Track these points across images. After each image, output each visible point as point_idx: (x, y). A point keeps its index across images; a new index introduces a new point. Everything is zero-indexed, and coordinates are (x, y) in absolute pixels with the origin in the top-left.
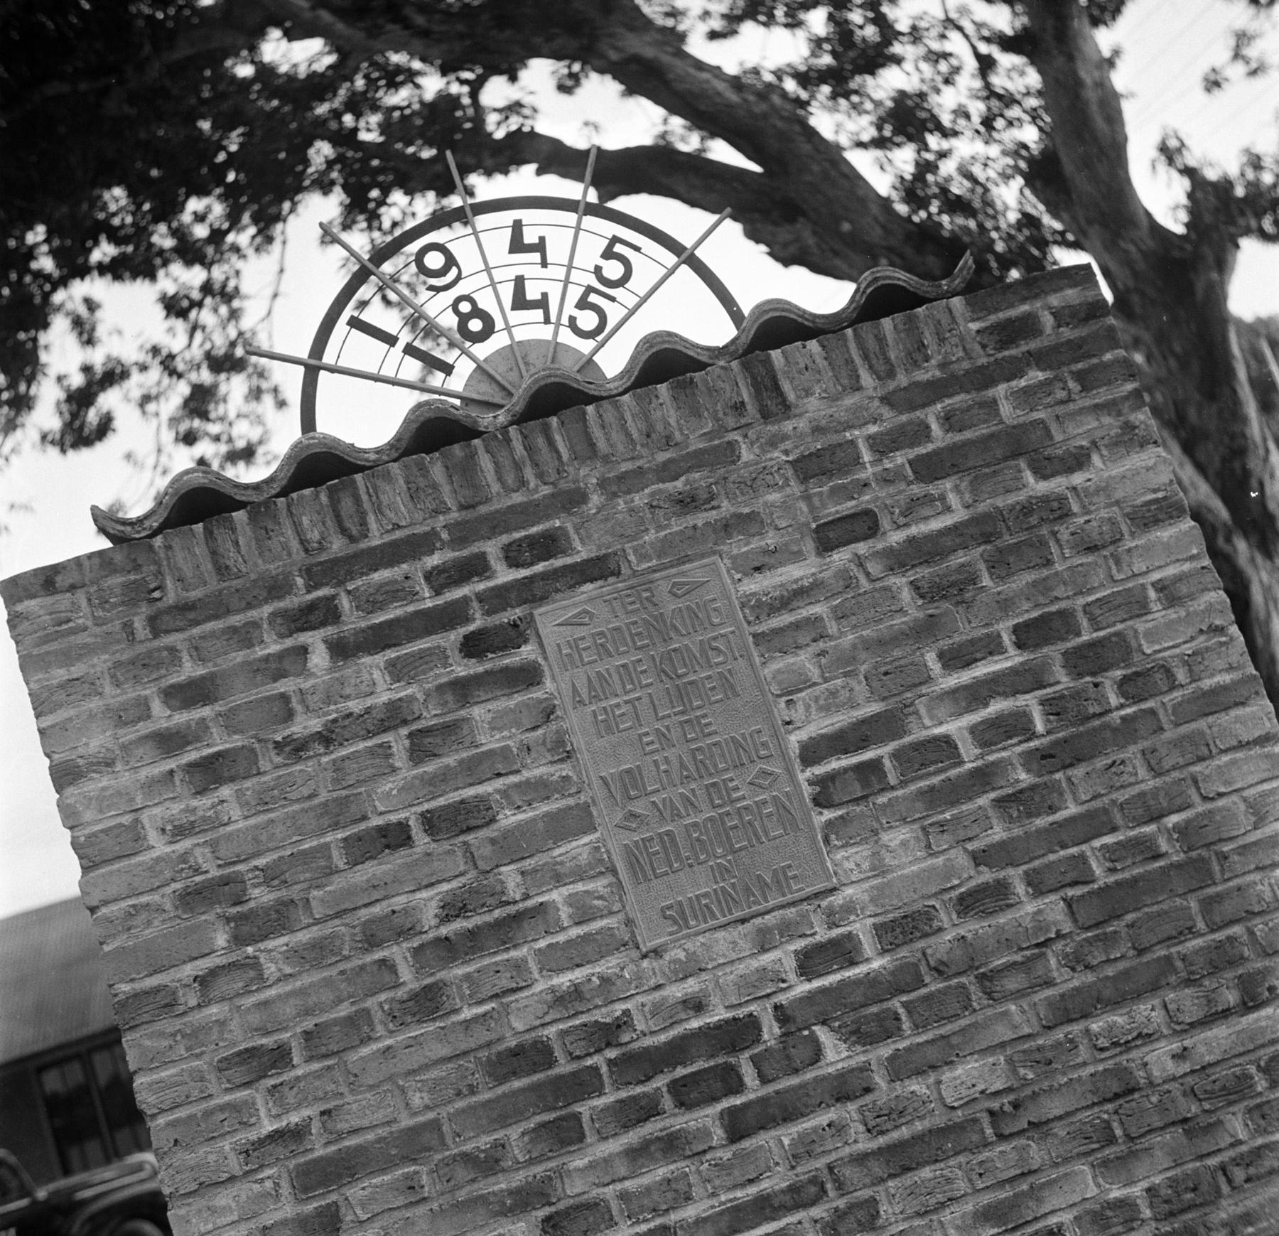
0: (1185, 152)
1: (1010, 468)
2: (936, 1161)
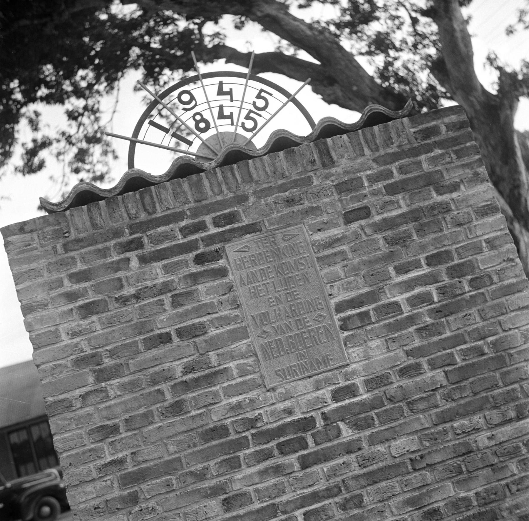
0: (497, 60)
1: (426, 190)
2: (388, 479)
